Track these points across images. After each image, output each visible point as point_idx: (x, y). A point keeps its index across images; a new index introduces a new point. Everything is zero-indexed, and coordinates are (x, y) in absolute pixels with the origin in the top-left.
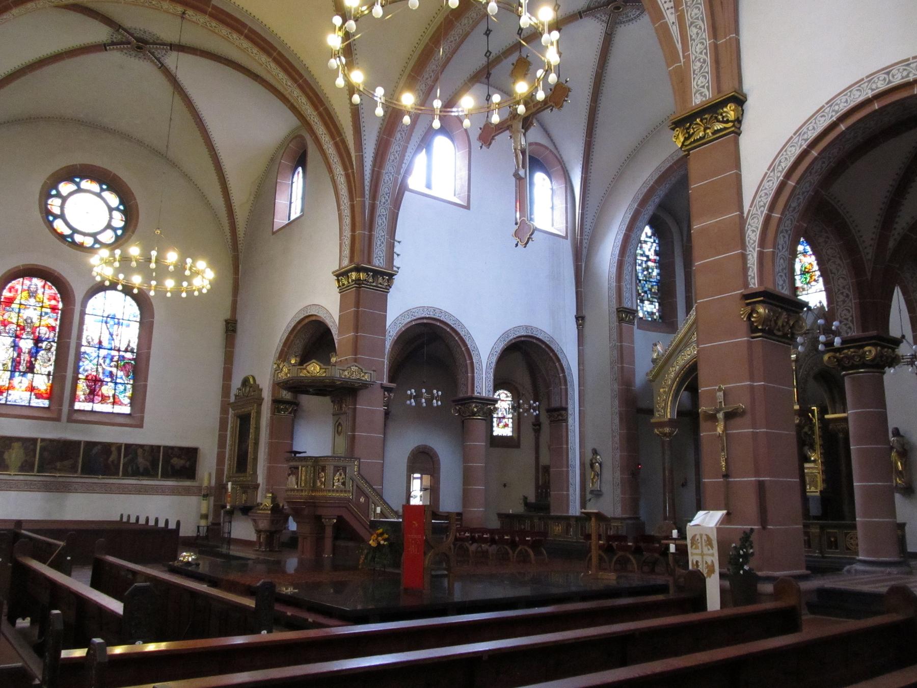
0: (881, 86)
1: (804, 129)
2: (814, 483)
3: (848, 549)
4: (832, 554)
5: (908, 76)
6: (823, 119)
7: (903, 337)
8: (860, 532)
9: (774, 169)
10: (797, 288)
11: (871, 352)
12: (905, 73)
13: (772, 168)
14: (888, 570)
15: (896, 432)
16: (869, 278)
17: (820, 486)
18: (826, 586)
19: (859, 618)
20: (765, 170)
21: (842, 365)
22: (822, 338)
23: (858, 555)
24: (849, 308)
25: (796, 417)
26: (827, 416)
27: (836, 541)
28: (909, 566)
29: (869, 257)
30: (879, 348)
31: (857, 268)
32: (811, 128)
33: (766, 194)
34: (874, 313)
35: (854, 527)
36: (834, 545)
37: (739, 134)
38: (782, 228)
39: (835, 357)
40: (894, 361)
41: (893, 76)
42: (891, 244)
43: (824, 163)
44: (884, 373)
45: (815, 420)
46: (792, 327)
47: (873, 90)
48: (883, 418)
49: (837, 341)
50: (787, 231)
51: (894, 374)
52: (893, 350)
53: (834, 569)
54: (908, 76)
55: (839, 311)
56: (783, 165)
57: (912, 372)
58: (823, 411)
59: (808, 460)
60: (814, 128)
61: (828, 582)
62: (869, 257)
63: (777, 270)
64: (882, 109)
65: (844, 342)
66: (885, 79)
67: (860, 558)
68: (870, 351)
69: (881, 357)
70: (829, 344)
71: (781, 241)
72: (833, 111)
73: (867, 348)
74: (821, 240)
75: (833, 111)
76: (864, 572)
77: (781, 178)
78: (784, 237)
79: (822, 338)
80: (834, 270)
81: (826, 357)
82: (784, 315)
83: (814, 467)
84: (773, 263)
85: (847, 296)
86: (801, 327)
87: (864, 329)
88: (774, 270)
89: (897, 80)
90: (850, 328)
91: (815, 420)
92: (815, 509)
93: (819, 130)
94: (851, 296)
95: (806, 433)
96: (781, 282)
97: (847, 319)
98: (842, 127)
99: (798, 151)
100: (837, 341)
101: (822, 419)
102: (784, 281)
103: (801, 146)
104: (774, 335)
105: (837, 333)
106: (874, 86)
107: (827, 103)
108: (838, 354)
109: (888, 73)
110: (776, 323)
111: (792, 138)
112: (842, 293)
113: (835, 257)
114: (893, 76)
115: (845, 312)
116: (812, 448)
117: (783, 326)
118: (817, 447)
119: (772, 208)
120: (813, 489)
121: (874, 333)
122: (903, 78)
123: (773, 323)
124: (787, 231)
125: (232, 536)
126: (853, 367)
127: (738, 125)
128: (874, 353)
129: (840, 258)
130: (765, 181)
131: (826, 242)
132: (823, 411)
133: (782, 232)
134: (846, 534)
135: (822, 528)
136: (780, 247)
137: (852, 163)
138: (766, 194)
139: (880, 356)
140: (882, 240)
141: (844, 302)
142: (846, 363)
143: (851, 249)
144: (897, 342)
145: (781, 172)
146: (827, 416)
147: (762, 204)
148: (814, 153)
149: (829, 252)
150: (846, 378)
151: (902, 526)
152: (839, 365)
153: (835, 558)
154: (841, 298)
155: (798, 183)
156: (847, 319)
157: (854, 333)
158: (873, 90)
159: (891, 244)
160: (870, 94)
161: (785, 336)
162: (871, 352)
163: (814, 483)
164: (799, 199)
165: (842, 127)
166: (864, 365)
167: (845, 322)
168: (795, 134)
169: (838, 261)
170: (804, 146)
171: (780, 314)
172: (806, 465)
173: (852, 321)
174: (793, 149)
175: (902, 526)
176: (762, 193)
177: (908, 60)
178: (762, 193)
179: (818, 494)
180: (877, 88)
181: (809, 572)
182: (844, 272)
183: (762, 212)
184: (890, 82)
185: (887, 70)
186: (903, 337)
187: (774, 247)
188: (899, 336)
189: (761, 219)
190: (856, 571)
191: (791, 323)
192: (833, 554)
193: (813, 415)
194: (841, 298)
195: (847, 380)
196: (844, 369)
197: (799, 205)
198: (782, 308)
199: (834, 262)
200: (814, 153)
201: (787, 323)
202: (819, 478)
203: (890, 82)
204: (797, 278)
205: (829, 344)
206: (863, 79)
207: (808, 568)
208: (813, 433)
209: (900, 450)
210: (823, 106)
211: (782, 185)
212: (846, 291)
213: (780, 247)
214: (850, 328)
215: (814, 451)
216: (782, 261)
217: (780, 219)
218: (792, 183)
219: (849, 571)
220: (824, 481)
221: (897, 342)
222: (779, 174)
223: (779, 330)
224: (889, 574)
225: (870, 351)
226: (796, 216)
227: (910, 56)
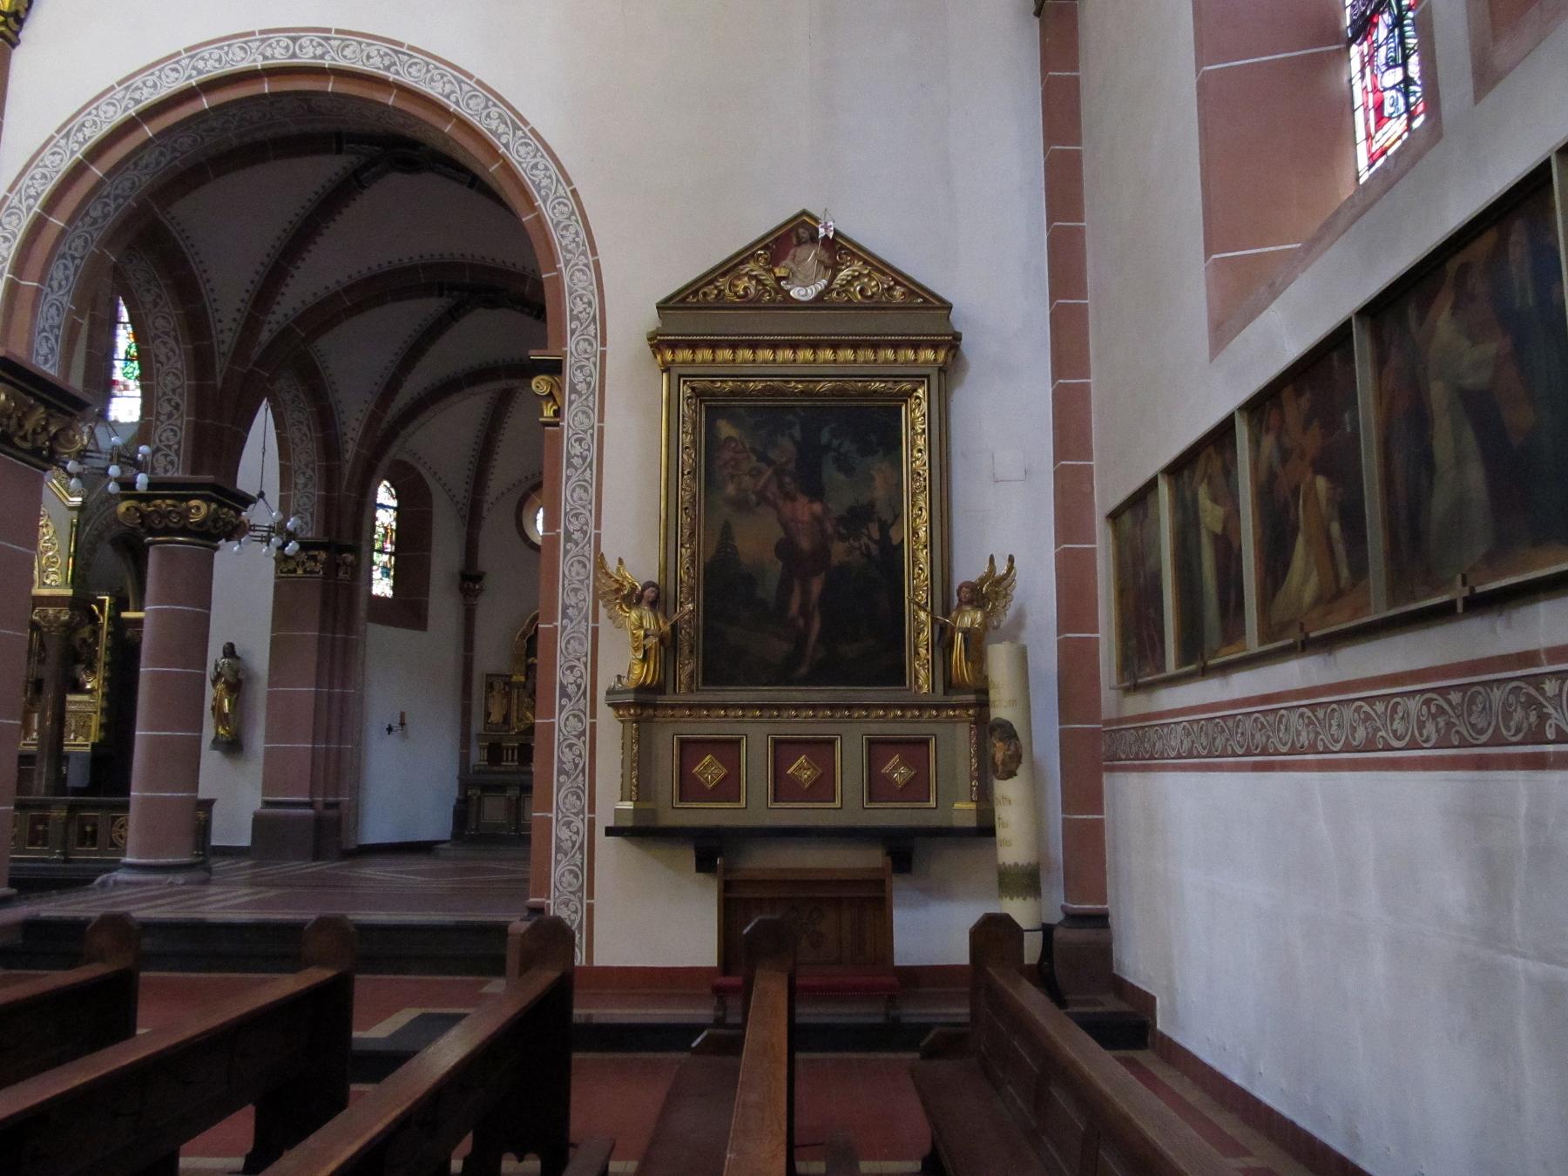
0: (280, 57)
1: (138, 81)
2: (83, 729)
3: (113, 844)
4: (83, 854)
5: (322, 57)
6: (175, 75)
7: (261, 495)
8: (133, 815)
9: (67, 136)
10: (114, 383)
11: (199, 510)
12: (319, 51)
13: (65, 130)
14: (171, 878)
15: (230, 651)
16: (219, 385)
17: (95, 735)
18: (43, 914)
19: (70, 967)
20: (52, 131)
21: (149, 525)
22: (114, 470)
23: (124, 855)
24: (176, 431)
25: (66, 610)
26: (125, 615)
27: (94, 832)
28: (209, 870)
29: (224, 348)
30: (214, 506)
31: (201, 363)
32: (150, 83)
33: (44, 176)
34: (217, 443)
35: (125, 807)
36: (88, 838)
37: (14, 45)
38: (63, 249)
39: (137, 509)
40: (235, 531)
41: (301, 47)
42: (265, 336)
43: (162, 154)
44: (216, 549)
45: (104, 620)
46: (54, 438)
47: (265, 58)
48: (201, 625)
49: (142, 480)
50: (73, 258)
51: (238, 553)
52: (238, 513)
53: (76, 882)
54: (322, 57)
55: (159, 431)
56: (87, 132)
57: (266, 555)
58: (121, 604)
59: (78, 688)
60: (155, 86)
61: (50, 908)
62: (224, 348)
63: (41, 323)
64: (276, 96)
65: (152, 485)
66: (287, 48)
67: (128, 860)
68: (198, 508)
69: (215, 521)
70: (127, 485)
71: (58, 273)
72: (194, 68)
73: (193, 503)
74: (149, 298)
75: (194, 68)
76: (129, 884)
77: (79, 155)
78: (66, 268)
79: (114, 470)
80: (162, 358)
81: (122, 507)
82: (41, 411)
83: (87, 704)
84: (34, 315)
85: (177, 407)
86: (72, 442)
87: (196, 468)
88: (33, 325)
89: (306, 58)
90: (172, 463)
91: (104, 620)
92: (76, 775)
93: (164, 92)
94: (184, 407)
95: (84, 640)
96: (44, 350)
97: (169, 447)
98: (205, 103)
99: (118, 117)
100: (142, 480)
101: (115, 619)
102: (52, 350)
103: (127, 109)
104: (13, 445)
105: (140, 467)
106: (269, 52)
107: (186, 50)
108: (143, 505)
109: (294, 40)
110: (20, 426)
111: (112, 88)
112: (169, 401)
113: (167, 334)
114: (301, 47)
115: (170, 434)
116: (91, 668)
117: (34, 432)
118: (100, 666)
119: (52, 203)
120: (80, 740)
121: (207, 478)
122: (314, 57)
123: (13, 422)
124: (73, 258)
125: (1105, 776)
126: (167, 531)
127: (15, 27)
128: (204, 510)
129: (176, 339)
130: (47, 151)
131: (156, 304)
132: (121, 604)
133: (63, 256)
134: (115, 819)
135: (72, 808)
136: (55, 284)
137: (217, 176)
138: (44, 176)
139: (213, 518)
140: (251, 324)
141: (170, 416)
142: (157, 523)
143: (196, 325)
144: (246, 501)
145: (81, 144)
146: (125, 615)
147: (32, 192)
148: (148, 131)
149: (160, 322)
150: (151, 549)
151: (207, 805)
152: (142, 524)
153: (87, 861)
154: (167, 408)
155: (108, 174)
156: (169, 447)
157: (177, 474)
158: (265, 58)
159: (265, 336)
160: (260, 64)
161: (36, 452)
162: (199, 510)
163: (83, 729)
164: (106, 205)
165: (205, 103)
166: (183, 531)
167: (167, 451)
168: (119, 84)
169: (172, 343)
170: (132, 112)
171: (32, 408)
172: (70, 698)
173: (177, 452)
174: (112, 109)
175: (207, 805)
176: (38, 173)
177: (328, 30)
178: (38, 173)
179: (88, 749)
180: (273, 57)
181: (14, 891)
182: (179, 365)
183: (29, 208)
184: (294, 55)
185: (294, 34)
186: (261, 495)
187: (41, 280)
188: (253, 492)
189: (26, 221)
190: (116, 883)
191: (53, 430)
192: (85, 855)
193: (102, 611)
194: (167, 408)
195: (152, 552)
196: (153, 532)
197: (105, 216)
198: (38, 399)
199: (165, 343)
200: (148, 131)
201: (45, 428)
202: (95, 721)
203: (294, 55)
204: (119, 364)
205: (127, 485)
206: (253, 33)
207: (12, 883)
208: (97, 643)
209: (230, 679)
210: (179, 53)
211: (78, 170)
212: (177, 399)
213: (55, 284)
214: (172, 463)
215: (94, 673)
216: (53, 311)
217: (63, 232)
218: (97, 171)
219: (104, 884)
220: (102, 726)
221: (246, 501)
222: (76, 147)
223: (24, 438)
224: (171, 884)
225: (198, 508)
226: (97, 235)
227: (334, 26)
